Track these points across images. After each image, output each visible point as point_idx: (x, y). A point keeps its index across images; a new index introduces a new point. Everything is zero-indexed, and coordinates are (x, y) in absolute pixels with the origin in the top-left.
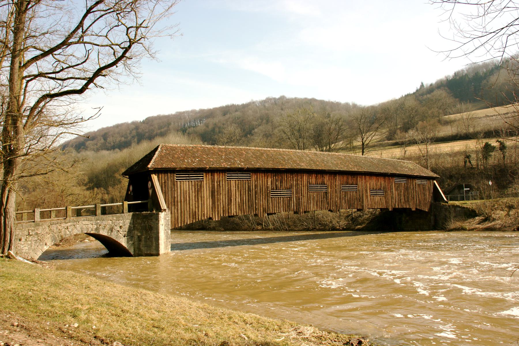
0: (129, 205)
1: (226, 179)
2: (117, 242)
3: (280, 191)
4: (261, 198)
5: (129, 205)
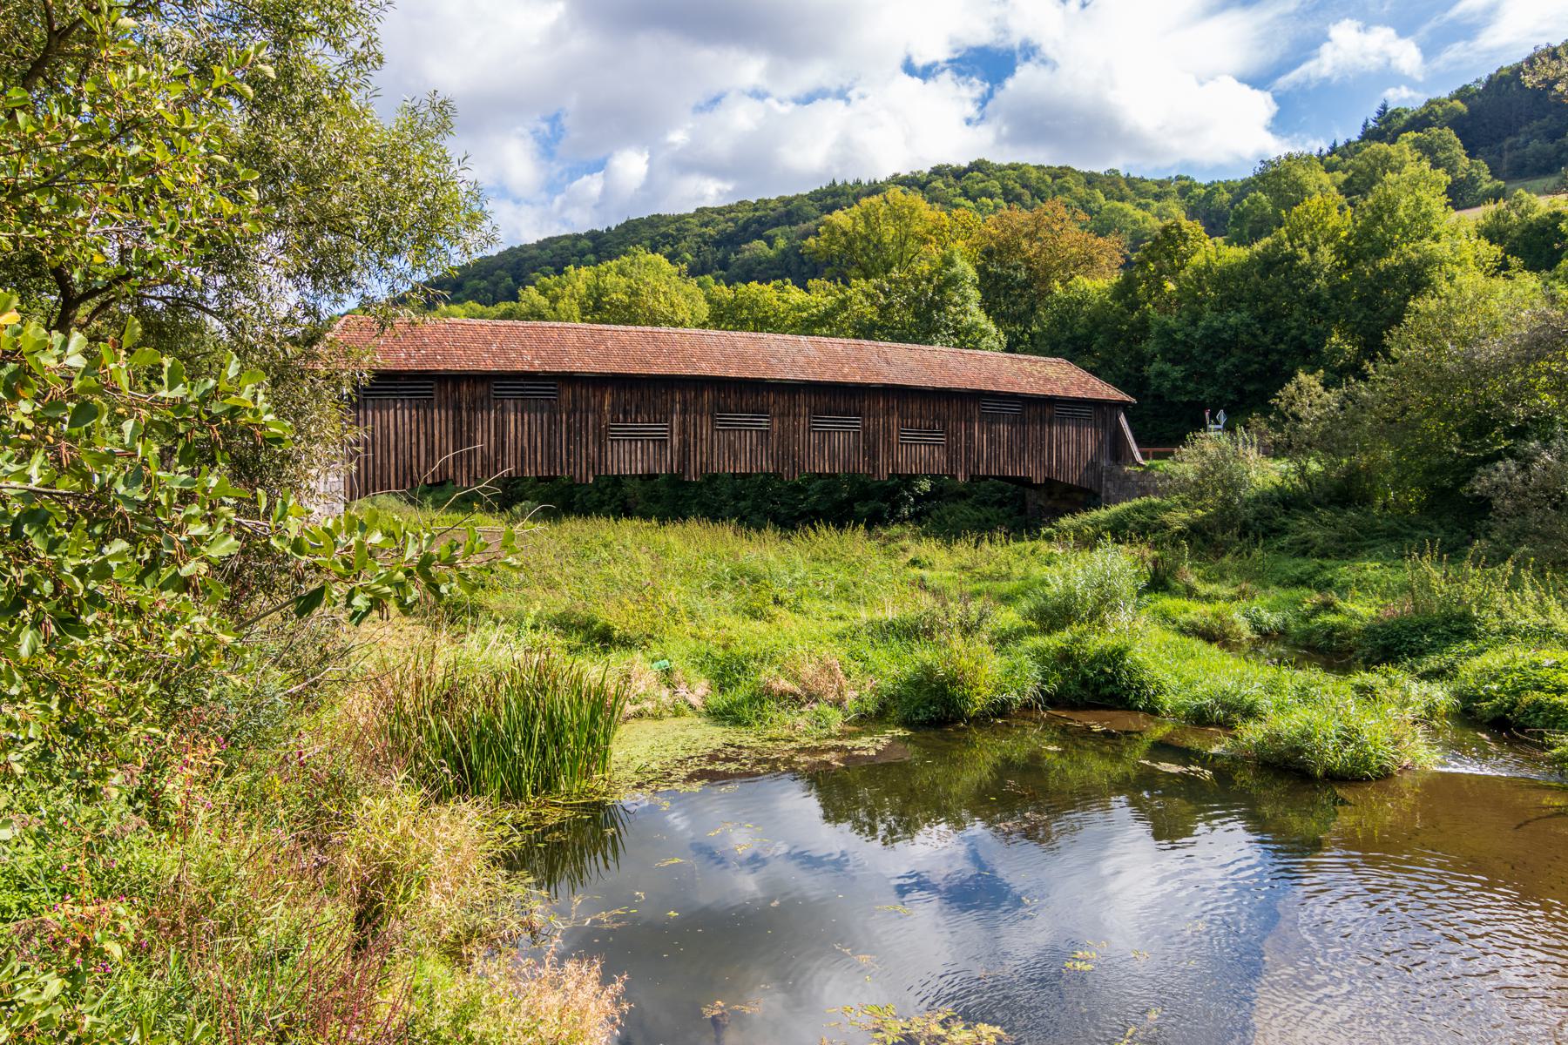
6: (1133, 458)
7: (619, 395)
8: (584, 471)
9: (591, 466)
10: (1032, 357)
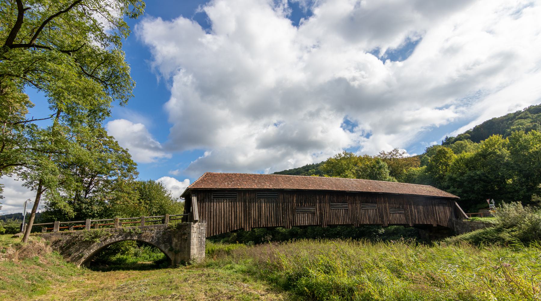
1: (257, 198)
4: (288, 213)
10: (418, 185)
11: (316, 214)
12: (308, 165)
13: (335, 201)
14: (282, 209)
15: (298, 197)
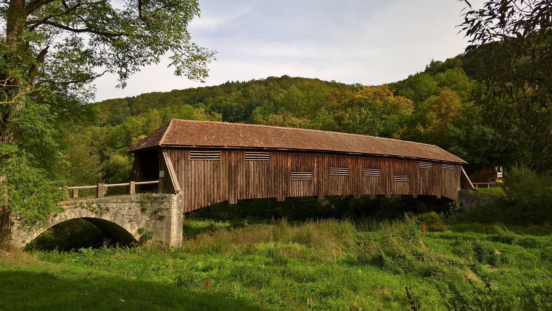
0: (136, 185)
2: (121, 227)
3: (338, 169)
5: (136, 185)
6: (471, 186)
7: (294, 159)
8: (281, 195)
9: (284, 193)
10: (423, 144)
11: (313, 182)
12: (230, 82)
13: (336, 165)
14: (274, 175)
15: (294, 159)
